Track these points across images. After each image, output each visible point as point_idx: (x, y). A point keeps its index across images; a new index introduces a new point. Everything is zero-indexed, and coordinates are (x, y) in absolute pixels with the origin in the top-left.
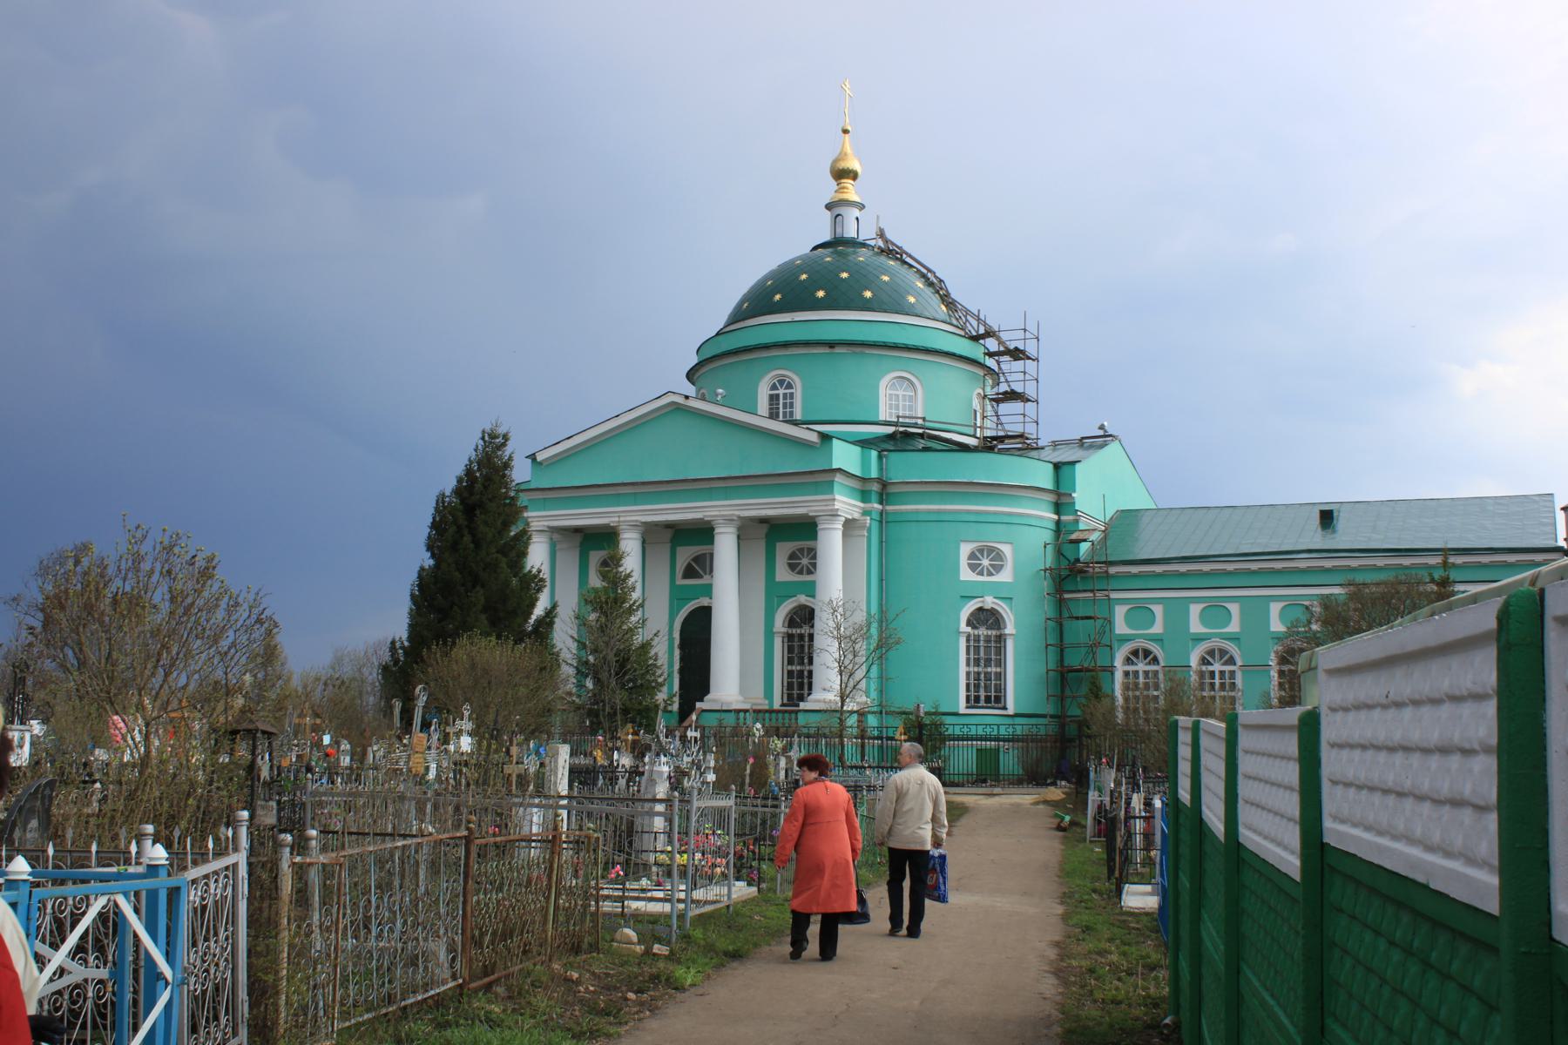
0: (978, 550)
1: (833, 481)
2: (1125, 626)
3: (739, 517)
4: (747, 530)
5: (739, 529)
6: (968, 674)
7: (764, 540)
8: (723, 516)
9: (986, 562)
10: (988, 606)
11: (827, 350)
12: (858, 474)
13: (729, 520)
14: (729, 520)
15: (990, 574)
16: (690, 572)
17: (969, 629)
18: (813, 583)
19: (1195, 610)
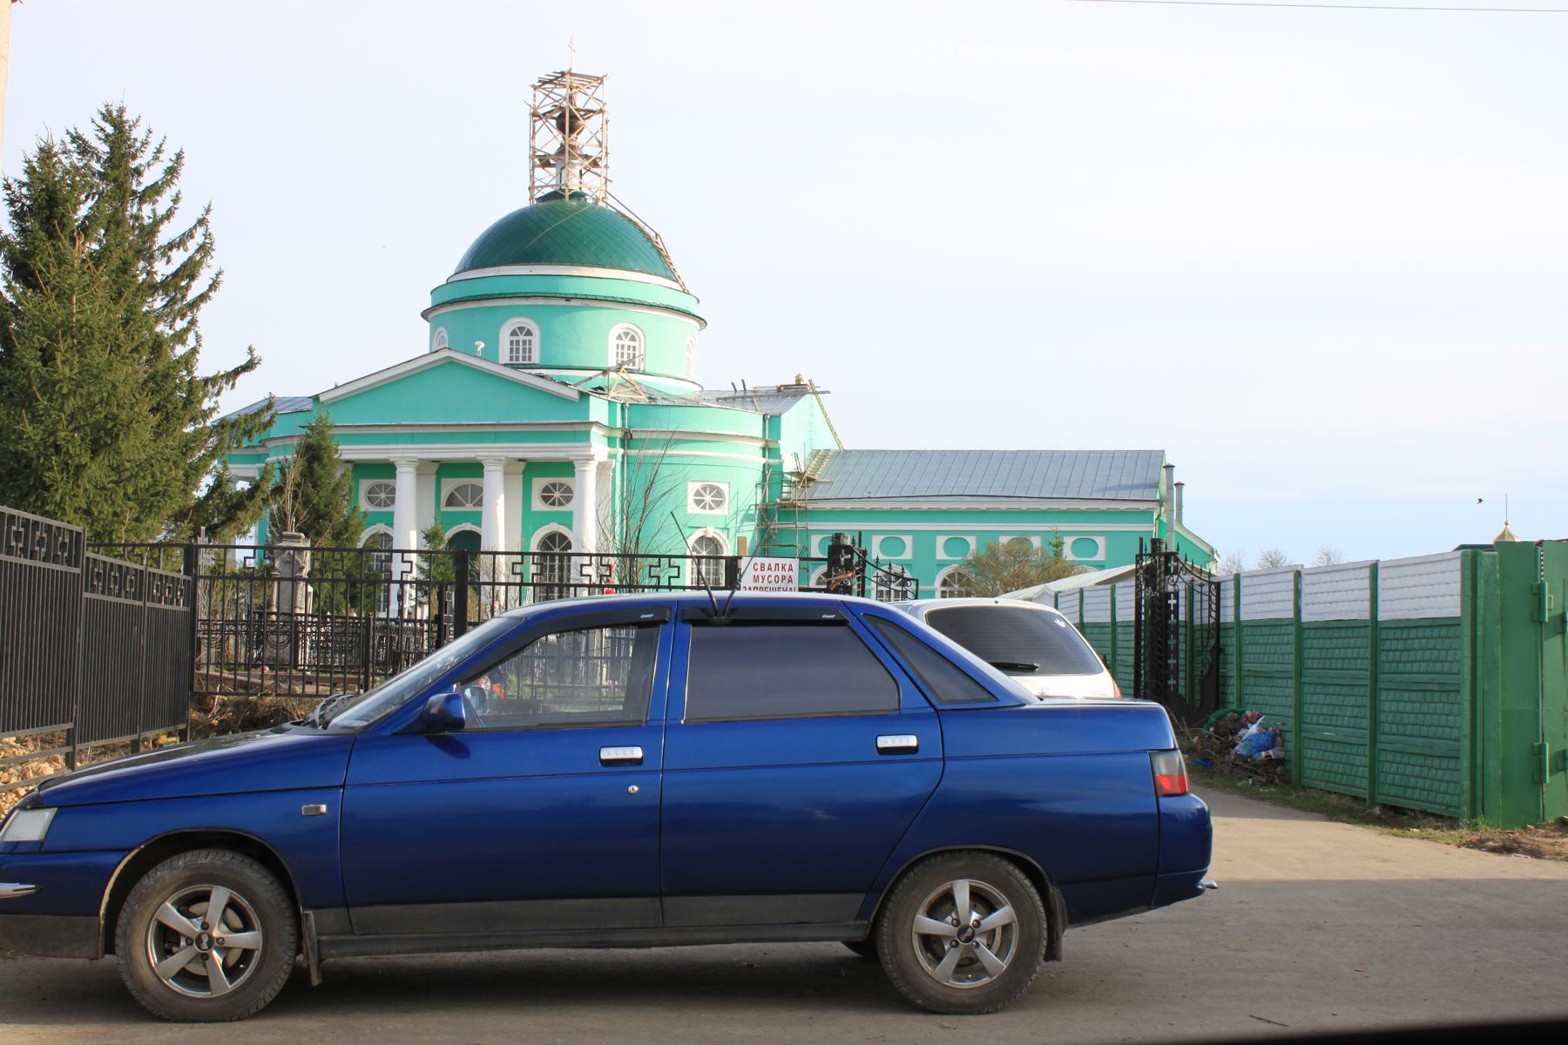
1: (589, 432)
2: (818, 551)
3: (507, 458)
4: (422, 467)
5: (505, 467)
6: (944, 595)
7: (521, 476)
8: (494, 456)
10: (709, 535)
11: (564, 303)
12: (607, 424)
13: (497, 460)
14: (497, 460)
16: (451, 501)
18: (392, 514)
19: (941, 540)
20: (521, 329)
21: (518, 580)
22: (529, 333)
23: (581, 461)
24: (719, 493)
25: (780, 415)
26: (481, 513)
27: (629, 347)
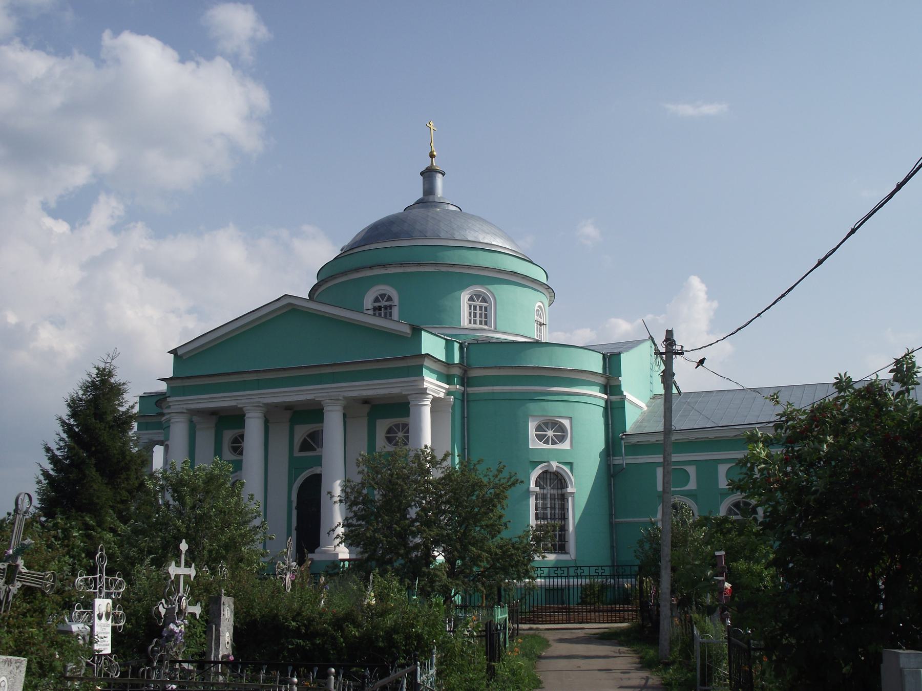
0: (543, 423)
9: (550, 433)
11: (399, 265)
15: (554, 443)
16: (305, 446)
17: (538, 489)
20: (383, 296)
21: (597, 574)
22: (390, 299)
23: (414, 396)
24: (562, 428)
25: (619, 354)
26: (241, 461)
27: (481, 307)
